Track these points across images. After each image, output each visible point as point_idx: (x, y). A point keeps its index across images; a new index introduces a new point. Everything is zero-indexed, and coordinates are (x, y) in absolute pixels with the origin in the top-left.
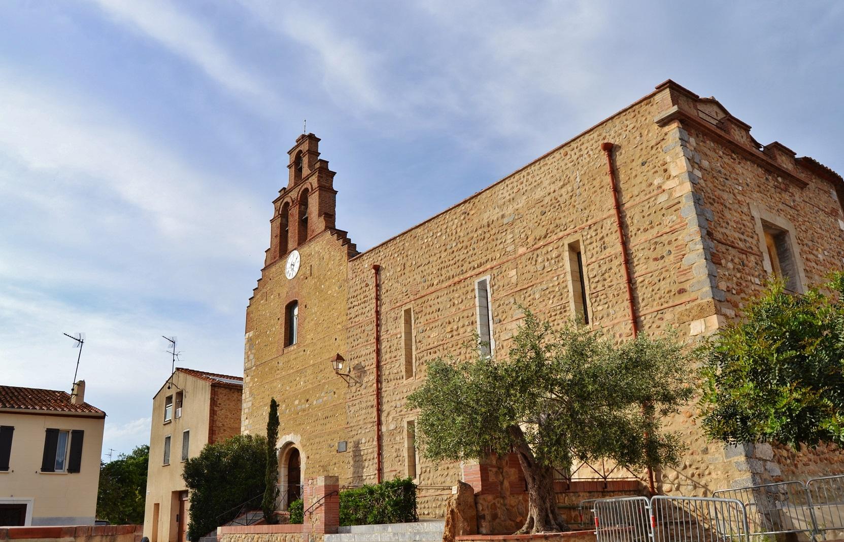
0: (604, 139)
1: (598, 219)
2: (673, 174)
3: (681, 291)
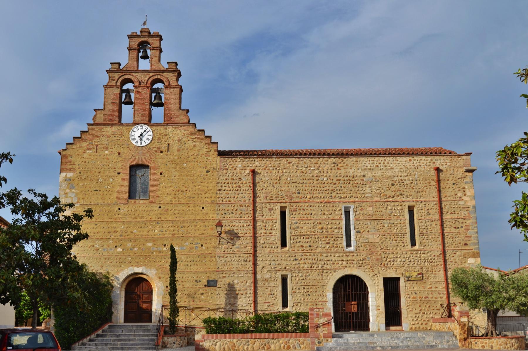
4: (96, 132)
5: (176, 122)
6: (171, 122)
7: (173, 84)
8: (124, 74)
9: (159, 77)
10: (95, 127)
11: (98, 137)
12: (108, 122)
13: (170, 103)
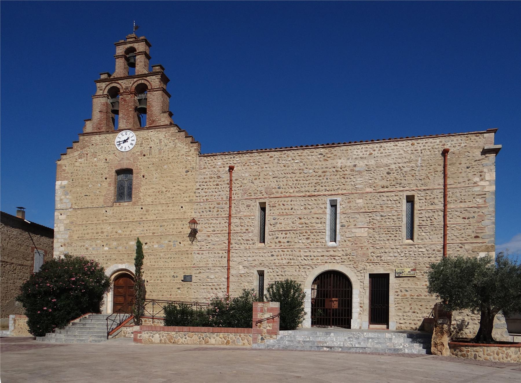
0: (444, 145)
1: (431, 188)
2: (487, 179)
3: (476, 237)
4: (87, 141)
5: (157, 125)
6: (153, 125)
10: (85, 137)
11: (88, 146)
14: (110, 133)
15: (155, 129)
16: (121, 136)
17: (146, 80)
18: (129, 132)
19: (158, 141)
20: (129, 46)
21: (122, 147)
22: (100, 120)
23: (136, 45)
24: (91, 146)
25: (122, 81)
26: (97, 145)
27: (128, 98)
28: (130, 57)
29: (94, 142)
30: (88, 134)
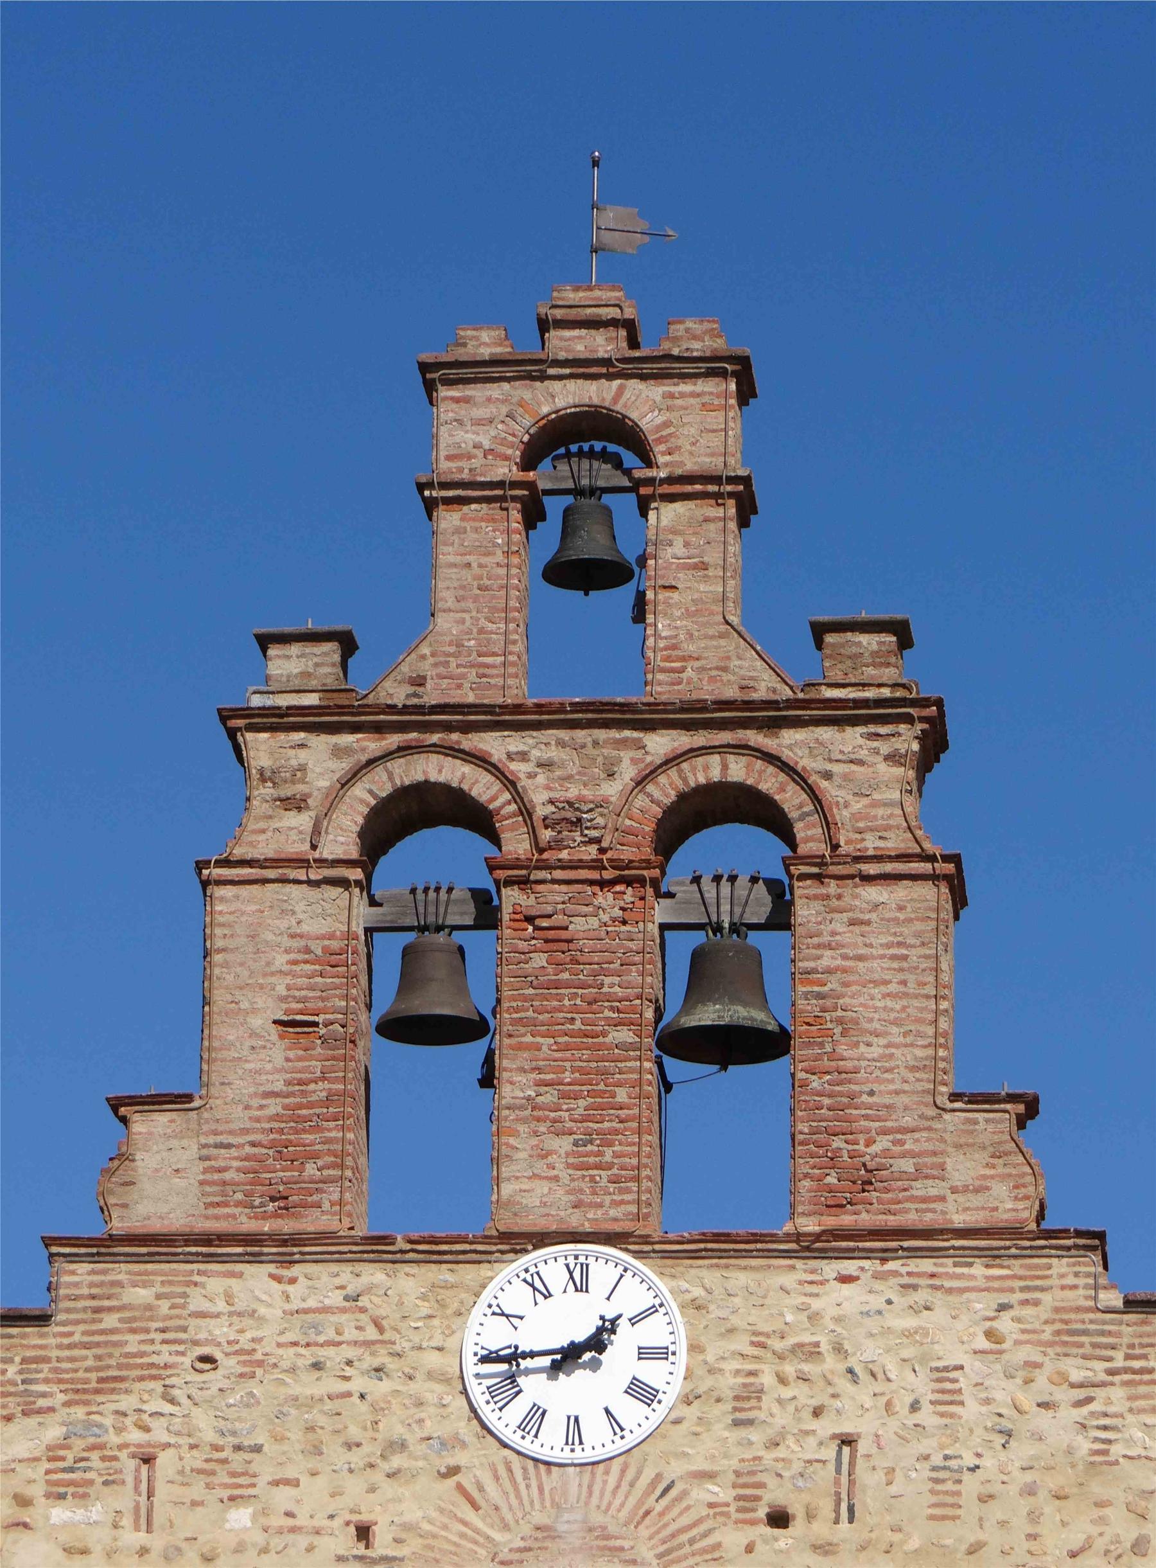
4: (137, 1320)
5: (910, 1218)
6: (865, 1219)
7: (871, 844)
8: (394, 740)
9: (738, 770)
10: (121, 1272)
11: (156, 1372)
12: (247, 1224)
13: (847, 1027)
14: (398, 1259)
15: (885, 1256)
16: (532, 1301)
17: (771, 758)
18: (604, 1264)
19: (922, 1385)
20: (566, 396)
21: (538, 1414)
22: (293, 1115)
23: (641, 402)
24: (184, 1379)
25: (515, 742)
26: (253, 1364)
27: (594, 917)
28: (582, 500)
29: (221, 1330)
30: (155, 1245)
